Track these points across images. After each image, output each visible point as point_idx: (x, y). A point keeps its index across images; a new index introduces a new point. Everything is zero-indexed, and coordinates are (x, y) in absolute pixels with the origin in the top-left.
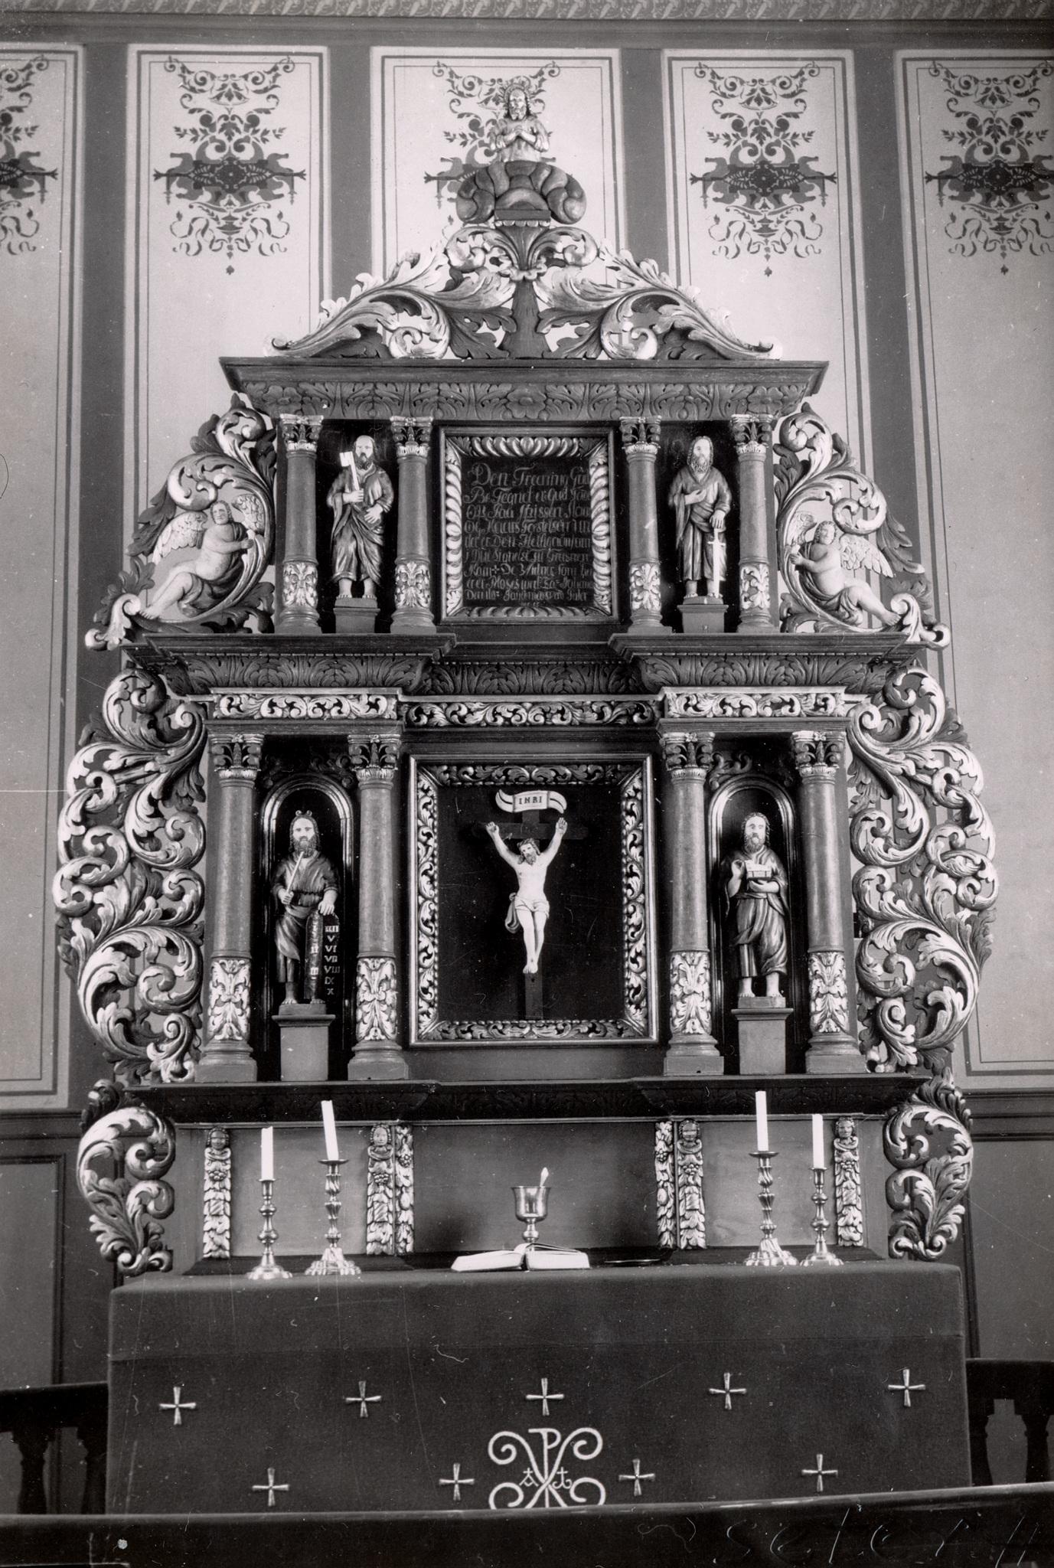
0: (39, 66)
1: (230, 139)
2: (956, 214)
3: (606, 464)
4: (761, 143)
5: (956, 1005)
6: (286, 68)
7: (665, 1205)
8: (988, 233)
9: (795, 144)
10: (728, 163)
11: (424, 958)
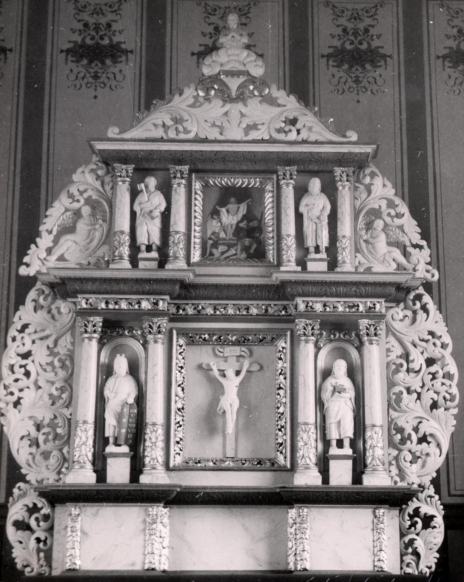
0: (381, 6)
1: (97, 34)
2: (73, 69)
3: (272, 191)
4: (356, 39)
5: (436, 454)
6: (254, 4)
7: (291, 549)
8: (350, 83)
9: (372, 40)
10: (340, 48)
11: (178, 427)
